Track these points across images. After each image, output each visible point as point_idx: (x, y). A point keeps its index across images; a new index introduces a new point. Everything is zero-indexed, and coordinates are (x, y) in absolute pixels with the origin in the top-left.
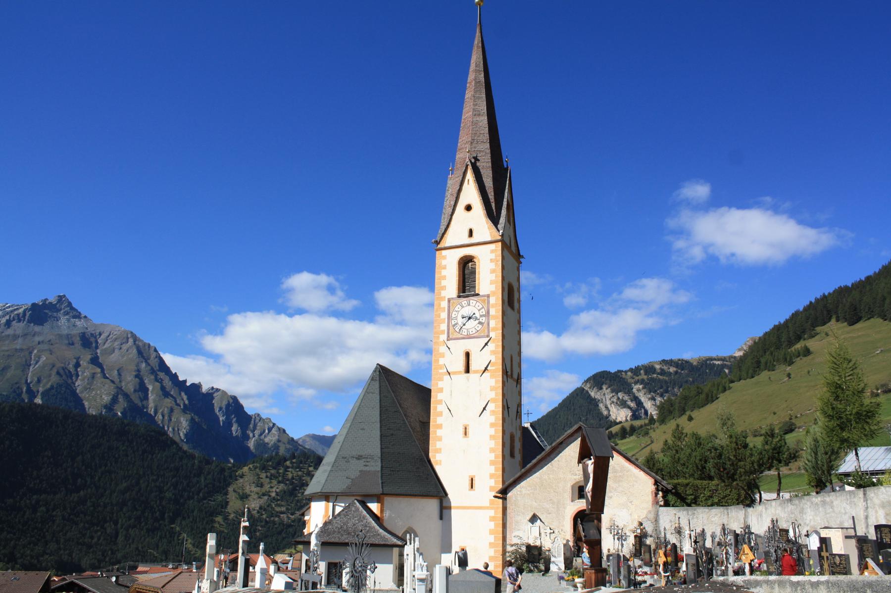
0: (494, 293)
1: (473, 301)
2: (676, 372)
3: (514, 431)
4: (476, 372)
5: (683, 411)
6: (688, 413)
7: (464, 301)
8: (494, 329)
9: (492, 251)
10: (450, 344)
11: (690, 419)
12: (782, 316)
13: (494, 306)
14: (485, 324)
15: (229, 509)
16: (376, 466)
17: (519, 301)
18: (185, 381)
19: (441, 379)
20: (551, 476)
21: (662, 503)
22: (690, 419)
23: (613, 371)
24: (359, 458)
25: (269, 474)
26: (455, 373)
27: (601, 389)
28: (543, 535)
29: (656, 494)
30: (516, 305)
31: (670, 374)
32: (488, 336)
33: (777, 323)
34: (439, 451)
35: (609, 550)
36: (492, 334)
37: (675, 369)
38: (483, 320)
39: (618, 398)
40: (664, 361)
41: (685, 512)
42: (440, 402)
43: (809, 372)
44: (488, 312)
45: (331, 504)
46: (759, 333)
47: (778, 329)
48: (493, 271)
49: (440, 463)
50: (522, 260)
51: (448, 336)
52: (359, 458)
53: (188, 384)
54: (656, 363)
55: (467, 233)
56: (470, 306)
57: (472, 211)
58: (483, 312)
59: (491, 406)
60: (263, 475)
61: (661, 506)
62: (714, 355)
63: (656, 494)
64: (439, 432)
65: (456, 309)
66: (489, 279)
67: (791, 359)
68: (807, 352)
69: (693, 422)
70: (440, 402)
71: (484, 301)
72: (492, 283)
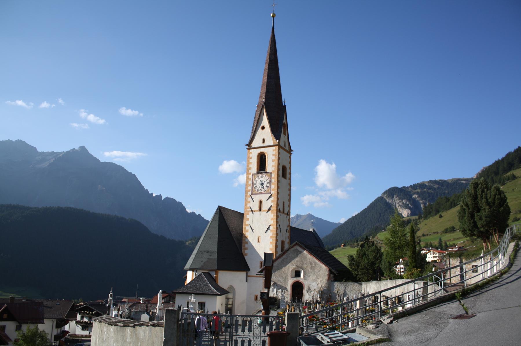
0: (274, 171)
1: (264, 175)
2: (438, 188)
3: (285, 240)
4: (264, 211)
5: (438, 212)
6: (440, 213)
7: (260, 176)
8: (273, 190)
9: (274, 150)
11: (441, 217)
12: (500, 156)
13: (274, 178)
16: (215, 256)
18: (152, 194)
22: (441, 217)
23: (400, 187)
24: (208, 252)
27: (393, 197)
30: (288, 176)
31: (435, 189)
33: (497, 160)
36: (272, 192)
37: (437, 186)
39: (403, 203)
40: (431, 181)
42: (247, 225)
43: (513, 190)
44: (271, 181)
45: (194, 273)
46: (487, 165)
47: (497, 163)
48: (274, 161)
50: (292, 152)
52: (208, 252)
53: (154, 195)
54: (426, 182)
55: (262, 141)
56: (264, 178)
57: (265, 130)
58: (269, 181)
59: (271, 228)
62: (461, 177)
66: (271, 165)
67: (504, 181)
68: (514, 177)
69: (442, 218)
70: (247, 225)
71: (269, 176)
72: (273, 166)
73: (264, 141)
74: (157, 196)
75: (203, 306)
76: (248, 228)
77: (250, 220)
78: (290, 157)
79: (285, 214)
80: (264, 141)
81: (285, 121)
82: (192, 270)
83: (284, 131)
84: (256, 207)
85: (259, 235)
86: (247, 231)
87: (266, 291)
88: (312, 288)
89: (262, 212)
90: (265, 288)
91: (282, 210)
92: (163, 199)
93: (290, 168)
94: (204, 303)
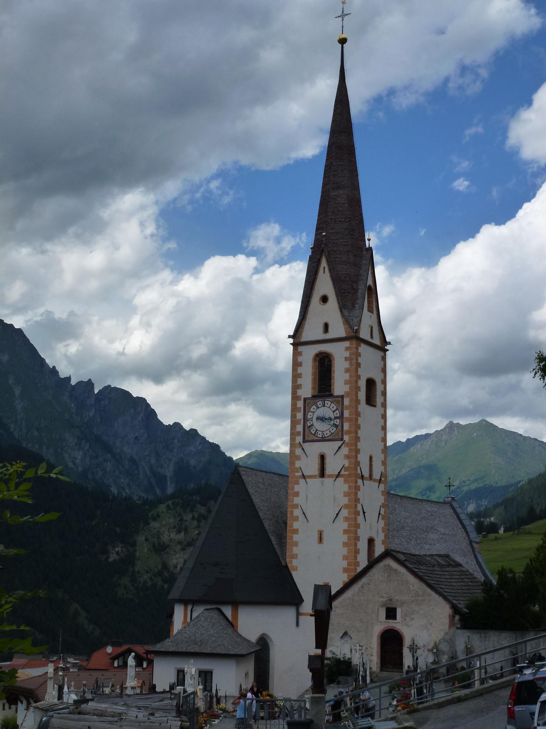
4: (330, 476)
10: (306, 446)
14: (340, 427)
15: (139, 566)
17: (384, 393)
18: (69, 379)
19: (297, 483)
20: (362, 598)
21: (459, 626)
25: (196, 515)
26: (311, 477)
28: (353, 651)
29: (453, 617)
30: (379, 399)
32: (342, 439)
34: (295, 556)
35: (409, 667)
38: (338, 422)
41: (478, 635)
42: (296, 506)
49: (296, 569)
50: (388, 347)
51: (304, 438)
53: (73, 382)
55: (321, 328)
60: (188, 517)
61: (458, 628)
63: (453, 617)
64: (296, 538)
65: (312, 410)
70: (296, 506)
71: (338, 402)
73: (326, 327)
74: (80, 383)
75: (208, 678)
76: (297, 512)
77: (302, 495)
78: (384, 359)
79: (375, 480)
80: (326, 327)
81: (370, 282)
82: (185, 602)
83: (370, 303)
84: (313, 468)
85: (321, 528)
86: (296, 519)
87: (319, 651)
88: (420, 643)
89: (326, 480)
90: (317, 647)
91: (366, 474)
92: (96, 391)
93: (384, 382)
94: (211, 673)
